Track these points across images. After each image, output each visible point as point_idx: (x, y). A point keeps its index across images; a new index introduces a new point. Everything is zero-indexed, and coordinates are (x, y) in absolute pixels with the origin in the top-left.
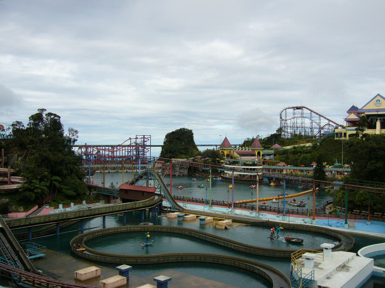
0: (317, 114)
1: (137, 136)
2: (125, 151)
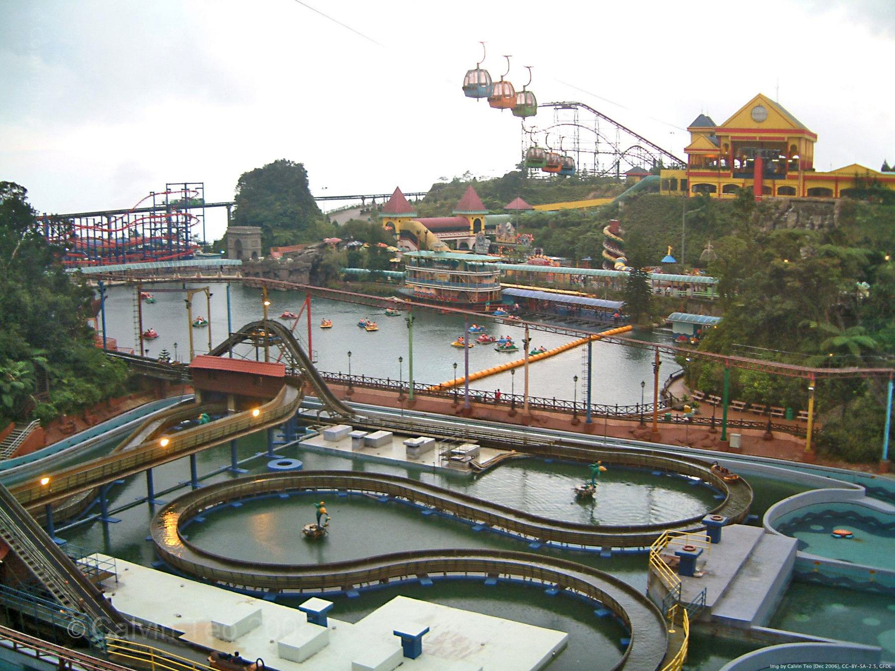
1: (169, 187)
2: (143, 229)
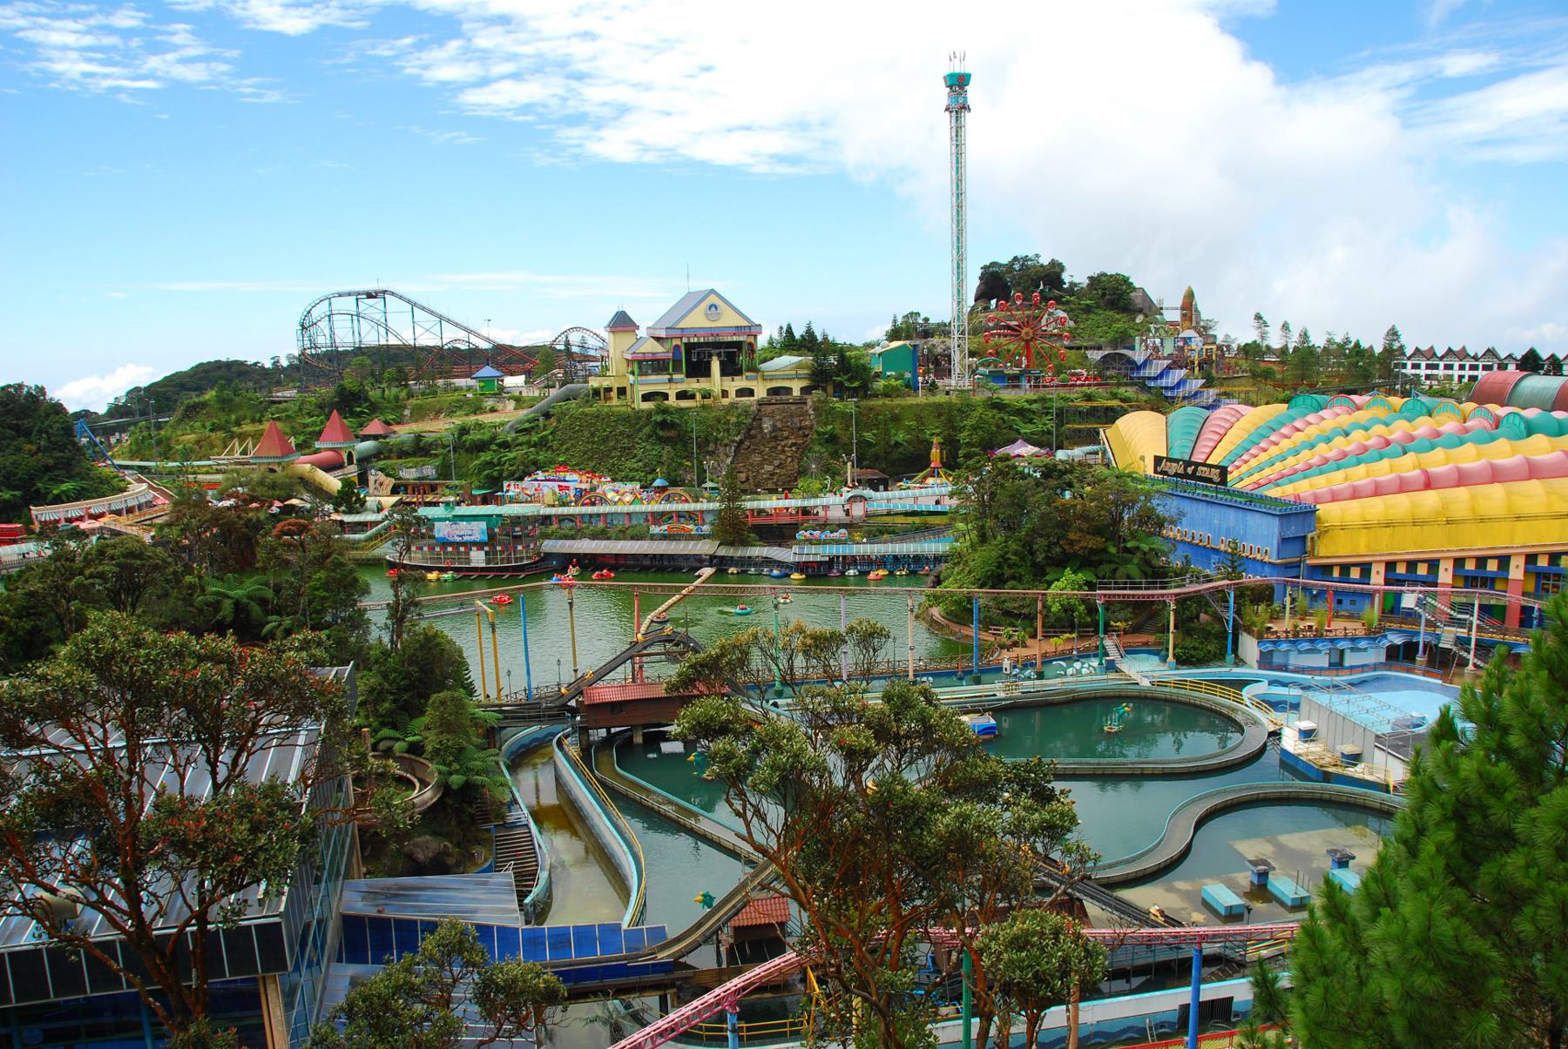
0: (432, 313)
